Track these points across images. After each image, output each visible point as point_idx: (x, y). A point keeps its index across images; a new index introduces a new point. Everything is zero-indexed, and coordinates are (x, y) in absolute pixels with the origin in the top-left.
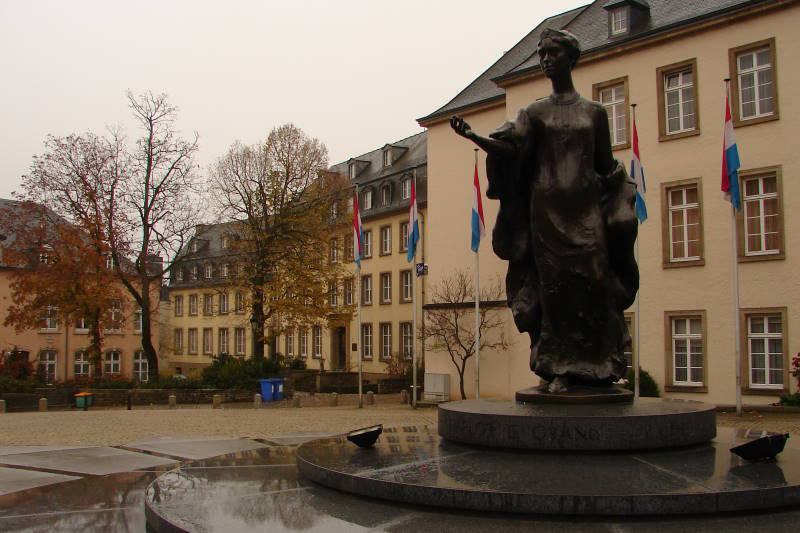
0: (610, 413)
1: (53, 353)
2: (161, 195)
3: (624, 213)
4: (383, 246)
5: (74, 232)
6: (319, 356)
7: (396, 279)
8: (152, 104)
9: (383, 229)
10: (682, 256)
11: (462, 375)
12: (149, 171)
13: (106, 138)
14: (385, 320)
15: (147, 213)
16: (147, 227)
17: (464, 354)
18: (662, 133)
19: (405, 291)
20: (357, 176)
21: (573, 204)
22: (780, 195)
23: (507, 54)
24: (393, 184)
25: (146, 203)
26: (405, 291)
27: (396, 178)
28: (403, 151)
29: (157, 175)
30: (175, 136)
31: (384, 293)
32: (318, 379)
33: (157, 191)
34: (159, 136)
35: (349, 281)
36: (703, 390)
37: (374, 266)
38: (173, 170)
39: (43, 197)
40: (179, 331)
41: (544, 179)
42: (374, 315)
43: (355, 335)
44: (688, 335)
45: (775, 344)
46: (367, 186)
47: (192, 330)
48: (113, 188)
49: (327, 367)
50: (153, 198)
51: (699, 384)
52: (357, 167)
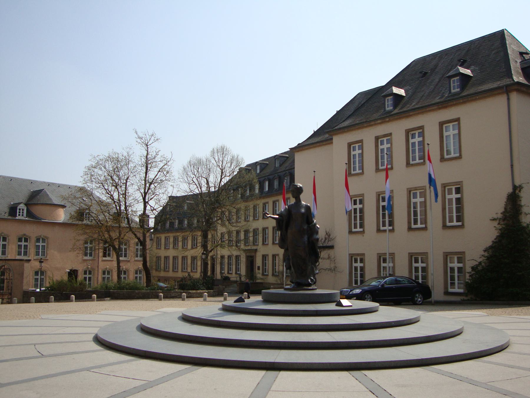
2: (152, 186)
5: (107, 205)
8: (148, 136)
10: (453, 222)
13: (121, 151)
14: (385, 250)
15: (145, 196)
16: (145, 203)
20: (260, 172)
22: (462, 196)
23: (338, 112)
25: (145, 191)
28: (285, 158)
29: (151, 175)
30: (160, 154)
33: (151, 184)
35: (255, 231)
38: (160, 173)
39: (91, 186)
40: (159, 258)
42: (226, 252)
43: (259, 262)
45: (424, 269)
47: (167, 258)
48: (126, 181)
49: (243, 279)
50: (148, 188)
52: (260, 166)
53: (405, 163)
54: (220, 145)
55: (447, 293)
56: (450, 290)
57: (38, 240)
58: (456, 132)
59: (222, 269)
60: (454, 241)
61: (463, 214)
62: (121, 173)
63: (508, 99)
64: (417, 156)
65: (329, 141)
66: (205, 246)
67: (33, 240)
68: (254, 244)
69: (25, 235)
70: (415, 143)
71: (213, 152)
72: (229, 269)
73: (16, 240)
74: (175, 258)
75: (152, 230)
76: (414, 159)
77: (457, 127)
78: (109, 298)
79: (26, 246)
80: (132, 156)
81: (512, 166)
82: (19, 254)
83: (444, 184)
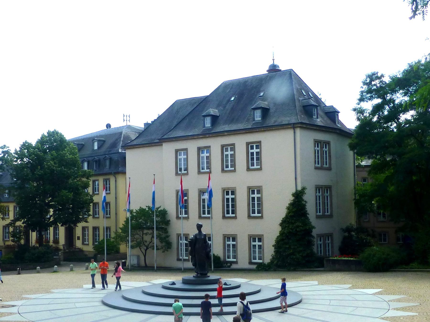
17: (145, 248)
22: (262, 196)
28: (102, 142)
36: (236, 263)
51: (235, 260)
53: (246, 168)
55: (251, 263)
58: (185, 157)
60: (111, 223)
63: (295, 133)
70: (228, 155)
74: (95, 229)
75: (366, 198)
76: (227, 167)
77: (186, 154)
81: (296, 178)
83: (249, 187)
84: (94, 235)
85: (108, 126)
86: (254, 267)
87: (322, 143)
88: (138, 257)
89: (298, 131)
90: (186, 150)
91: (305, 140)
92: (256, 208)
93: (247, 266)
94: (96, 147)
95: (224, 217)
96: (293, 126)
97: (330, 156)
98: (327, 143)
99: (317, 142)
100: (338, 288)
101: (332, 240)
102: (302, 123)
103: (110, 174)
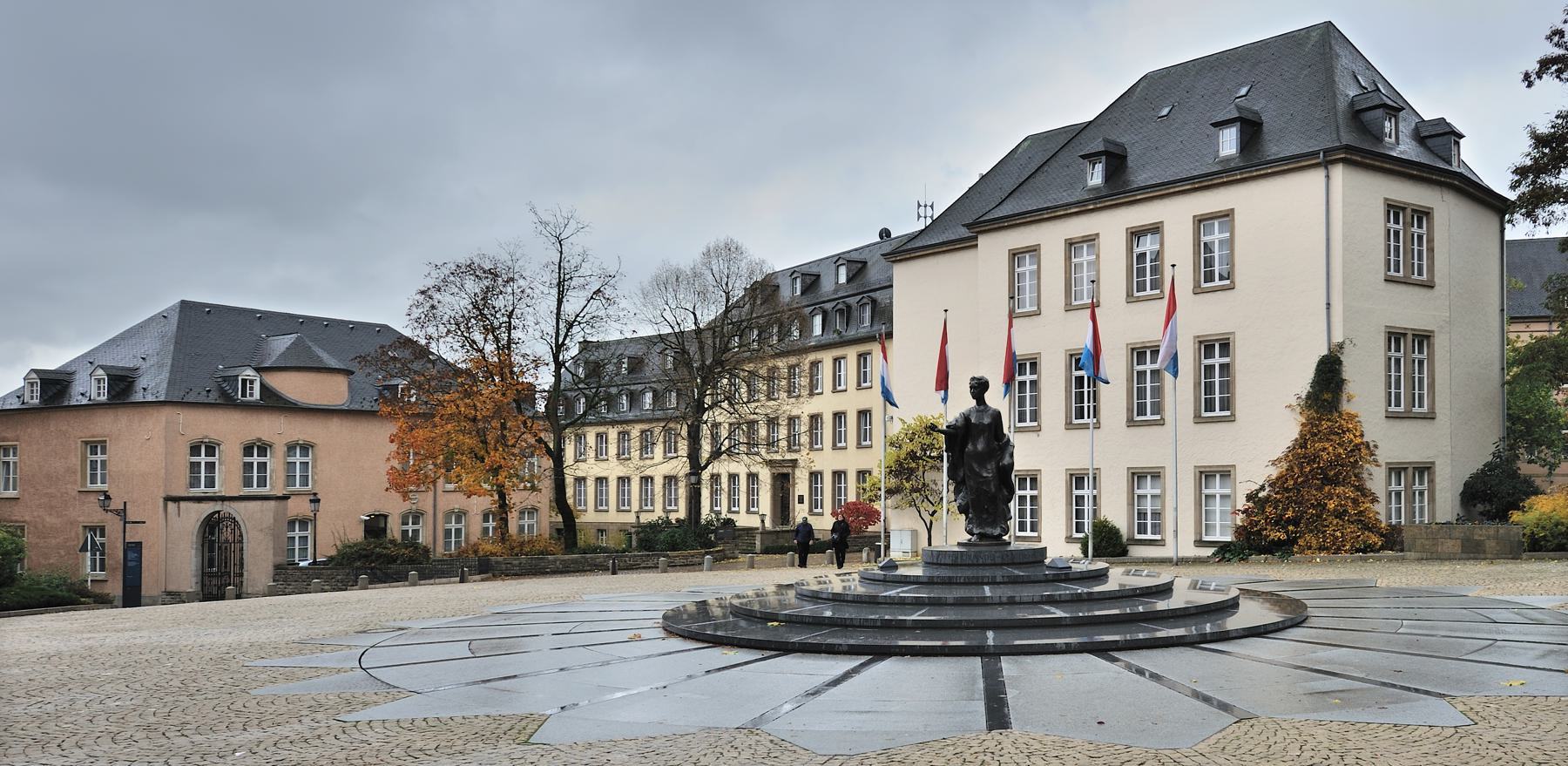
0: (1001, 548)
1: (417, 516)
3: (1006, 461)
4: (836, 380)
6: (755, 515)
7: (852, 420)
8: (560, 220)
9: (837, 360)
11: (929, 531)
12: (560, 302)
18: (1129, 295)
19: (864, 435)
21: (983, 458)
22: (1233, 360)
23: (983, 177)
24: (849, 307)
26: (864, 435)
27: (852, 301)
29: (571, 307)
31: (837, 437)
32: (758, 538)
33: (570, 326)
34: (572, 261)
36: (1160, 543)
37: (825, 404)
41: (970, 447)
42: (826, 460)
43: (801, 487)
44: (1148, 489)
46: (818, 307)
47: (601, 480)
51: (1158, 537)
52: (803, 282)
54: (722, 239)
55: (1200, 543)
56: (1206, 538)
57: (291, 448)
59: (714, 502)
61: (1233, 394)
62: (499, 303)
63: (1328, 177)
64: (1145, 275)
65: (968, 243)
66: (694, 455)
67: (280, 450)
68: (790, 450)
69: (259, 440)
71: (707, 254)
72: (733, 502)
73: (239, 452)
74: (838, 475)
78: (478, 577)
79: (262, 466)
80: (520, 263)
82: (248, 483)
84: (837, 491)
85: (885, 234)
86: (1209, 552)
87: (1409, 211)
88: (915, 533)
89: (1338, 172)
90: (1034, 250)
91: (1356, 197)
92: (1217, 398)
93: (1190, 551)
94: (843, 279)
95: (1131, 423)
96: (1325, 160)
97: (1431, 250)
98: (1423, 214)
99: (1394, 210)
100: (909, 246)
101: (1431, 481)
102: (1348, 148)
103: (870, 339)
